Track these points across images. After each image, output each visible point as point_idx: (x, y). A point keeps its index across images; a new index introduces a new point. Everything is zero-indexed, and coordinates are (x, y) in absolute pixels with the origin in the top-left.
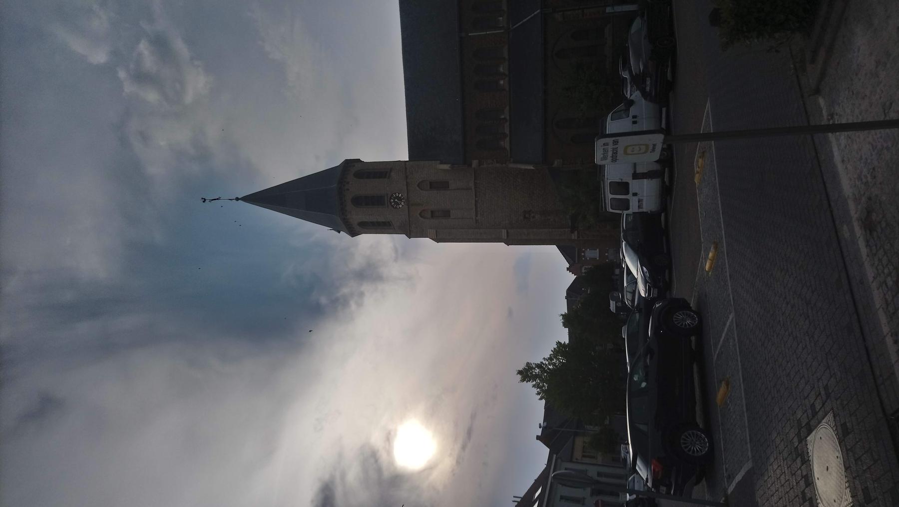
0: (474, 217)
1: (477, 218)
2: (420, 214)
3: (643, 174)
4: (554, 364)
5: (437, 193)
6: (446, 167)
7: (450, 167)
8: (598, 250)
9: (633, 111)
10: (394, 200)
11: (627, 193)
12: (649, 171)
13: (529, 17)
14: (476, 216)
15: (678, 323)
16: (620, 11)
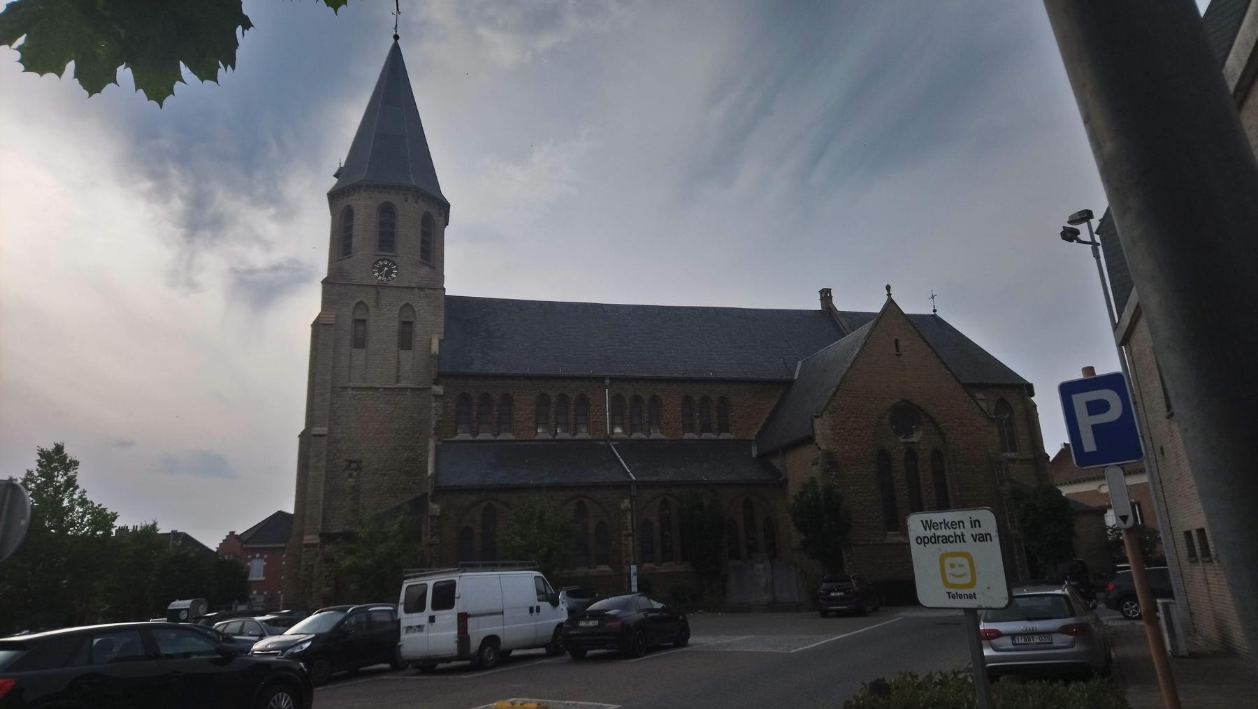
0: (351, 385)
1: (349, 389)
2: (361, 302)
3: (466, 628)
4: (71, 509)
5: (394, 332)
6: (435, 347)
7: (435, 352)
8: (263, 578)
9: (545, 606)
10: (386, 266)
11: (436, 606)
12: (469, 636)
13: (626, 467)
14: (353, 388)
15: (274, 702)
16: (632, 584)
